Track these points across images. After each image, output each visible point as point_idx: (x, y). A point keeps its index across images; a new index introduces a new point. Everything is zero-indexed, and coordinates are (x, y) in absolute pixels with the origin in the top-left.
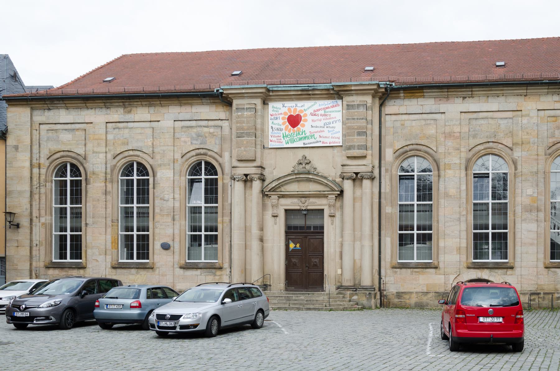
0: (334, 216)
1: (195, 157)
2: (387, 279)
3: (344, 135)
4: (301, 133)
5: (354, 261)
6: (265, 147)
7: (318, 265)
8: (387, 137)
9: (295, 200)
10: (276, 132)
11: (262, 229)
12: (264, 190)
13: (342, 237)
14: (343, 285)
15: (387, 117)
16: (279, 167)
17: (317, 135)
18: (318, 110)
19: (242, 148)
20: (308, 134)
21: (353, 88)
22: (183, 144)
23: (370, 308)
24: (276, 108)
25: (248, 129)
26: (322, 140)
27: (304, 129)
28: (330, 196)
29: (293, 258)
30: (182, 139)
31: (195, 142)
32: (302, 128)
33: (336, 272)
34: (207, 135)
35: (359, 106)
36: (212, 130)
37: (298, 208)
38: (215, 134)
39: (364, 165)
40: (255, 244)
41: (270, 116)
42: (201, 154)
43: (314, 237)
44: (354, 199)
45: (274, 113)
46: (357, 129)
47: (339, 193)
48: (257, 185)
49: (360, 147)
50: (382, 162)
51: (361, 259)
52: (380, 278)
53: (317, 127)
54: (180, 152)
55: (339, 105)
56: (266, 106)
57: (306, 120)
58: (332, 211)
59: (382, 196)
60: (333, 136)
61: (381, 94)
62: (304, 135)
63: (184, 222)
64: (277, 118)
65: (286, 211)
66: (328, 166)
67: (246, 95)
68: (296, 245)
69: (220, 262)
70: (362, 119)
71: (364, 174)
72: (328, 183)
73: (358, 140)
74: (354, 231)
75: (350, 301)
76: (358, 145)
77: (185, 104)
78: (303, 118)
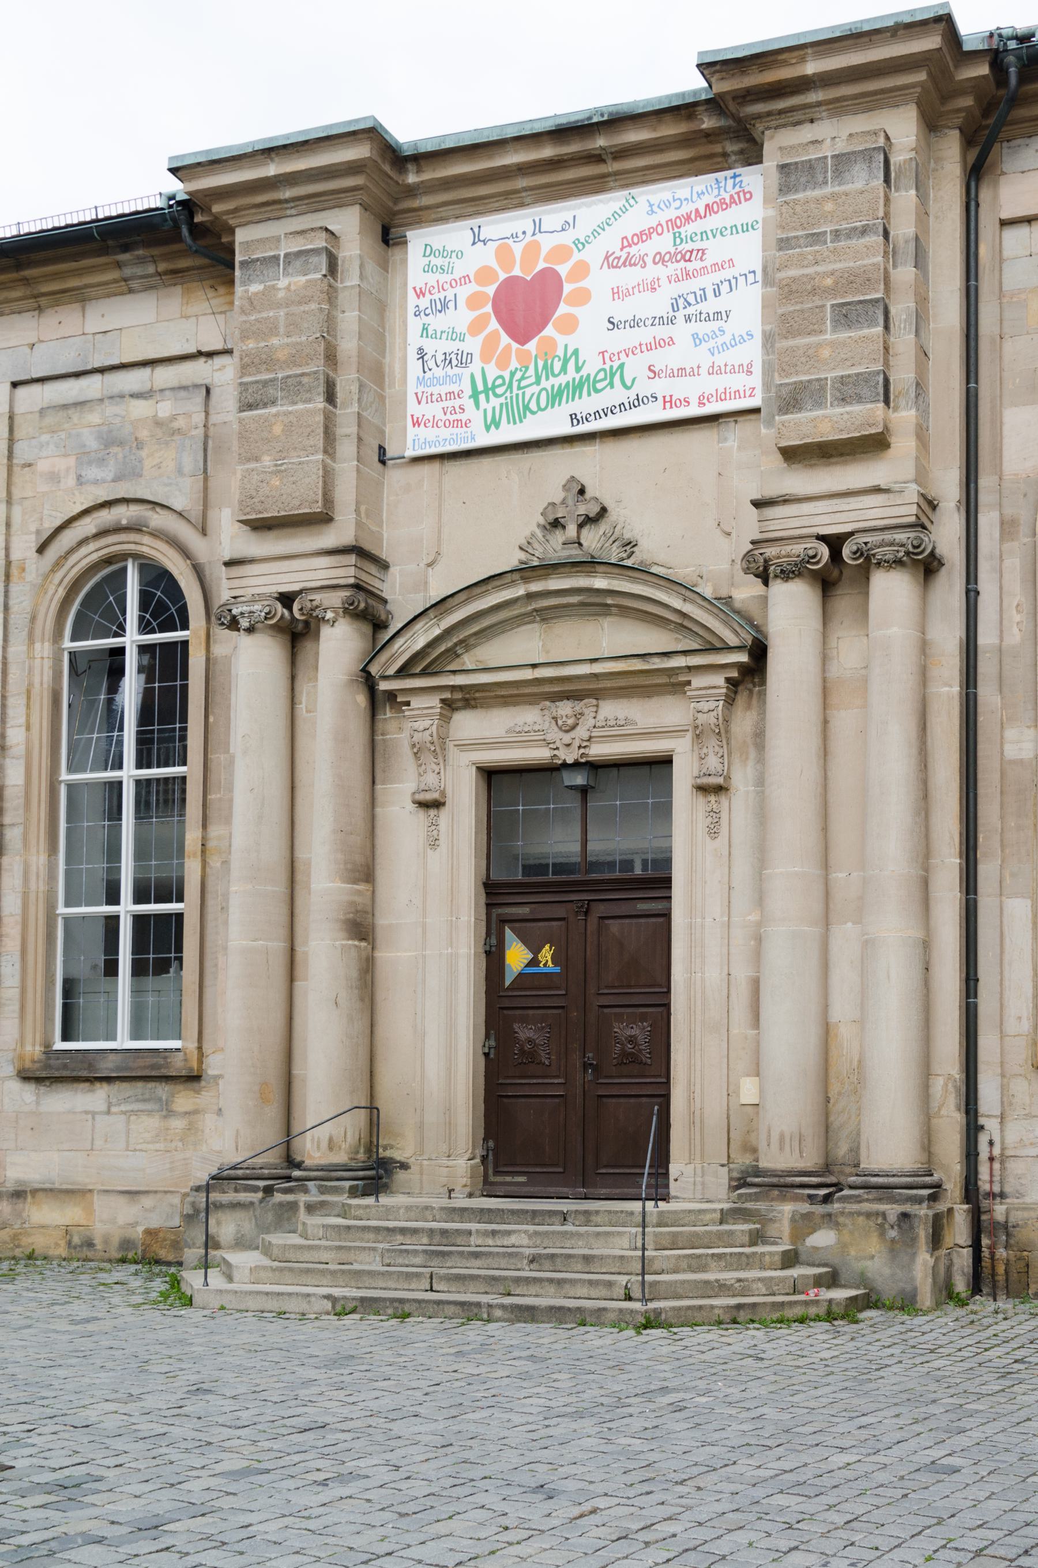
0: (719, 789)
1: (92, 546)
2: (1014, 1132)
3: (768, 340)
4: (557, 366)
5: (827, 1031)
6: (389, 454)
7: (645, 1057)
8: (1008, 346)
9: (528, 716)
10: (438, 372)
11: (364, 871)
12: (374, 669)
13: (760, 899)
14: (763, 1164)
15: (1013, 237)
16: (449, 543)
17: (635, 367)
18: (643, 236)
19: (267, 461)
20: (592, 366)
21: (811, 68)
22: (43, 488)
23: (906, 1303)
24: (443, 253)
25: (293, 361)
26: (661, 387)
27: (572, 341)
28: (698, 681)
29: (524, 1020)
30: (43, 466)
31: (92, 473)
32: (561, 340)
33: (731, 1091)
34: (144, 434)
35: (843, 162)
36: (165, 409)
37: (539, 754)
38: (180, 423)
39: (877, 490)
40: (325, 952)
41: (412, 300)
42: (118, 529)
43: (624, 909)
44: (826, 691)
45: (431, 279)
46: (833, 291)
47: (743, 658)
48: (339, 645)
49: (848, 390)
50: (986, 481)
51: (861, 1022)
52: (973, 1129)
53: (635, 323)
54: (33, 528)
55: (749, 196)
56: (395, 253)
57: (582, 297)
58: (713, 763)
59: (986, 667)
60: (720, 360)
61: (968, 102)
62: (571, 373)
63: (43, 858)
64: (445, 306)
65: (491, 776)
66: (688, 522)
67: (288, 193)
68: (536, 950)
69: (192, 1045)
70: (864, 231)
71: (872, 538)
72: (687, 608)
73: (842, 350)
74: (826, 865)
75: (790, 1259)
76: (842, 380)
77: (61, 298)
78: (567, 288)
